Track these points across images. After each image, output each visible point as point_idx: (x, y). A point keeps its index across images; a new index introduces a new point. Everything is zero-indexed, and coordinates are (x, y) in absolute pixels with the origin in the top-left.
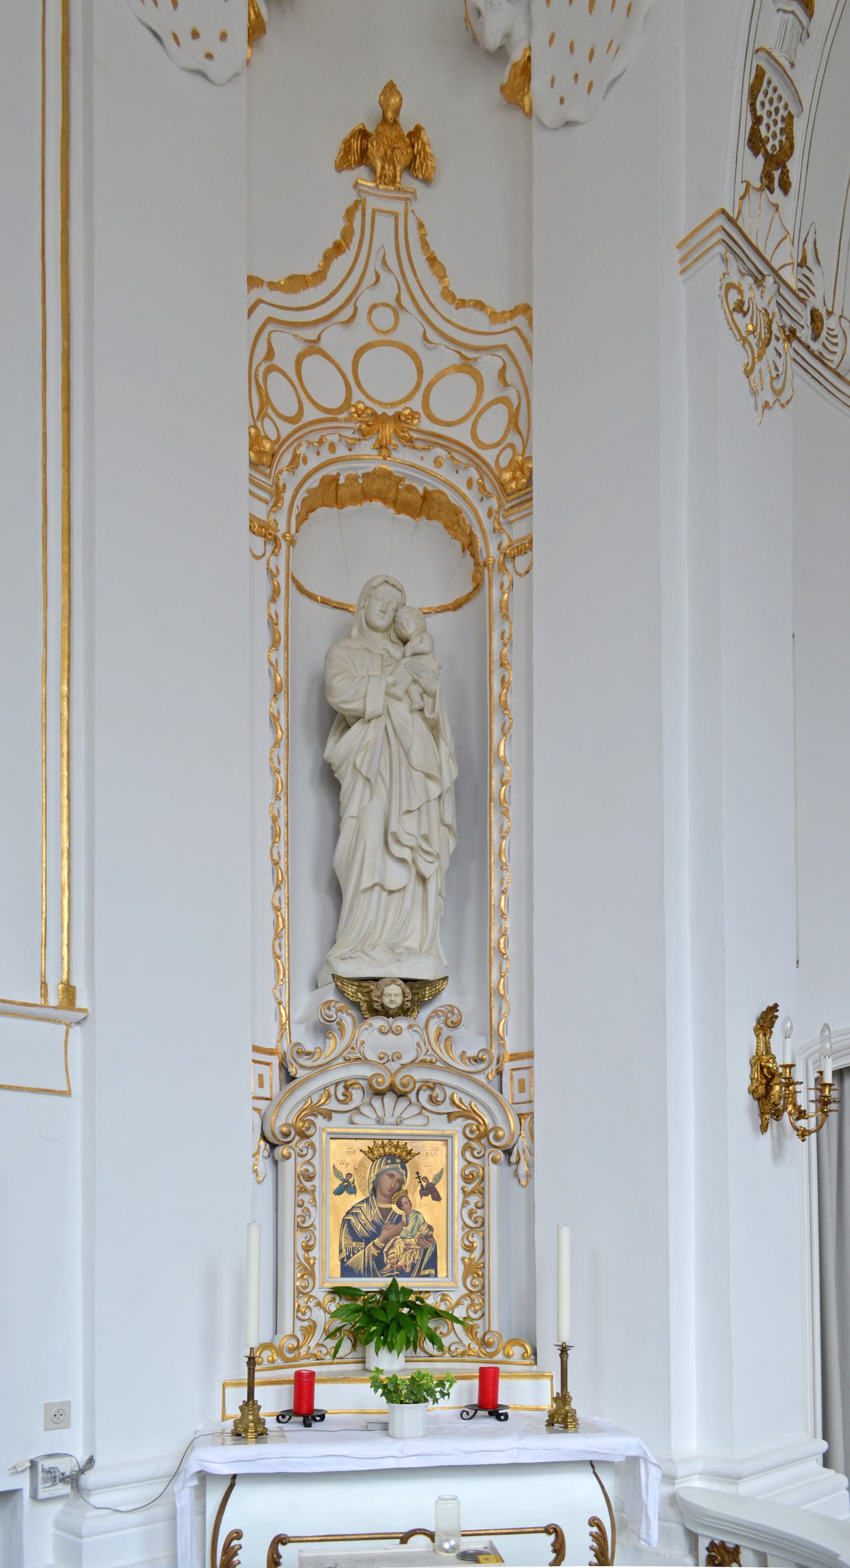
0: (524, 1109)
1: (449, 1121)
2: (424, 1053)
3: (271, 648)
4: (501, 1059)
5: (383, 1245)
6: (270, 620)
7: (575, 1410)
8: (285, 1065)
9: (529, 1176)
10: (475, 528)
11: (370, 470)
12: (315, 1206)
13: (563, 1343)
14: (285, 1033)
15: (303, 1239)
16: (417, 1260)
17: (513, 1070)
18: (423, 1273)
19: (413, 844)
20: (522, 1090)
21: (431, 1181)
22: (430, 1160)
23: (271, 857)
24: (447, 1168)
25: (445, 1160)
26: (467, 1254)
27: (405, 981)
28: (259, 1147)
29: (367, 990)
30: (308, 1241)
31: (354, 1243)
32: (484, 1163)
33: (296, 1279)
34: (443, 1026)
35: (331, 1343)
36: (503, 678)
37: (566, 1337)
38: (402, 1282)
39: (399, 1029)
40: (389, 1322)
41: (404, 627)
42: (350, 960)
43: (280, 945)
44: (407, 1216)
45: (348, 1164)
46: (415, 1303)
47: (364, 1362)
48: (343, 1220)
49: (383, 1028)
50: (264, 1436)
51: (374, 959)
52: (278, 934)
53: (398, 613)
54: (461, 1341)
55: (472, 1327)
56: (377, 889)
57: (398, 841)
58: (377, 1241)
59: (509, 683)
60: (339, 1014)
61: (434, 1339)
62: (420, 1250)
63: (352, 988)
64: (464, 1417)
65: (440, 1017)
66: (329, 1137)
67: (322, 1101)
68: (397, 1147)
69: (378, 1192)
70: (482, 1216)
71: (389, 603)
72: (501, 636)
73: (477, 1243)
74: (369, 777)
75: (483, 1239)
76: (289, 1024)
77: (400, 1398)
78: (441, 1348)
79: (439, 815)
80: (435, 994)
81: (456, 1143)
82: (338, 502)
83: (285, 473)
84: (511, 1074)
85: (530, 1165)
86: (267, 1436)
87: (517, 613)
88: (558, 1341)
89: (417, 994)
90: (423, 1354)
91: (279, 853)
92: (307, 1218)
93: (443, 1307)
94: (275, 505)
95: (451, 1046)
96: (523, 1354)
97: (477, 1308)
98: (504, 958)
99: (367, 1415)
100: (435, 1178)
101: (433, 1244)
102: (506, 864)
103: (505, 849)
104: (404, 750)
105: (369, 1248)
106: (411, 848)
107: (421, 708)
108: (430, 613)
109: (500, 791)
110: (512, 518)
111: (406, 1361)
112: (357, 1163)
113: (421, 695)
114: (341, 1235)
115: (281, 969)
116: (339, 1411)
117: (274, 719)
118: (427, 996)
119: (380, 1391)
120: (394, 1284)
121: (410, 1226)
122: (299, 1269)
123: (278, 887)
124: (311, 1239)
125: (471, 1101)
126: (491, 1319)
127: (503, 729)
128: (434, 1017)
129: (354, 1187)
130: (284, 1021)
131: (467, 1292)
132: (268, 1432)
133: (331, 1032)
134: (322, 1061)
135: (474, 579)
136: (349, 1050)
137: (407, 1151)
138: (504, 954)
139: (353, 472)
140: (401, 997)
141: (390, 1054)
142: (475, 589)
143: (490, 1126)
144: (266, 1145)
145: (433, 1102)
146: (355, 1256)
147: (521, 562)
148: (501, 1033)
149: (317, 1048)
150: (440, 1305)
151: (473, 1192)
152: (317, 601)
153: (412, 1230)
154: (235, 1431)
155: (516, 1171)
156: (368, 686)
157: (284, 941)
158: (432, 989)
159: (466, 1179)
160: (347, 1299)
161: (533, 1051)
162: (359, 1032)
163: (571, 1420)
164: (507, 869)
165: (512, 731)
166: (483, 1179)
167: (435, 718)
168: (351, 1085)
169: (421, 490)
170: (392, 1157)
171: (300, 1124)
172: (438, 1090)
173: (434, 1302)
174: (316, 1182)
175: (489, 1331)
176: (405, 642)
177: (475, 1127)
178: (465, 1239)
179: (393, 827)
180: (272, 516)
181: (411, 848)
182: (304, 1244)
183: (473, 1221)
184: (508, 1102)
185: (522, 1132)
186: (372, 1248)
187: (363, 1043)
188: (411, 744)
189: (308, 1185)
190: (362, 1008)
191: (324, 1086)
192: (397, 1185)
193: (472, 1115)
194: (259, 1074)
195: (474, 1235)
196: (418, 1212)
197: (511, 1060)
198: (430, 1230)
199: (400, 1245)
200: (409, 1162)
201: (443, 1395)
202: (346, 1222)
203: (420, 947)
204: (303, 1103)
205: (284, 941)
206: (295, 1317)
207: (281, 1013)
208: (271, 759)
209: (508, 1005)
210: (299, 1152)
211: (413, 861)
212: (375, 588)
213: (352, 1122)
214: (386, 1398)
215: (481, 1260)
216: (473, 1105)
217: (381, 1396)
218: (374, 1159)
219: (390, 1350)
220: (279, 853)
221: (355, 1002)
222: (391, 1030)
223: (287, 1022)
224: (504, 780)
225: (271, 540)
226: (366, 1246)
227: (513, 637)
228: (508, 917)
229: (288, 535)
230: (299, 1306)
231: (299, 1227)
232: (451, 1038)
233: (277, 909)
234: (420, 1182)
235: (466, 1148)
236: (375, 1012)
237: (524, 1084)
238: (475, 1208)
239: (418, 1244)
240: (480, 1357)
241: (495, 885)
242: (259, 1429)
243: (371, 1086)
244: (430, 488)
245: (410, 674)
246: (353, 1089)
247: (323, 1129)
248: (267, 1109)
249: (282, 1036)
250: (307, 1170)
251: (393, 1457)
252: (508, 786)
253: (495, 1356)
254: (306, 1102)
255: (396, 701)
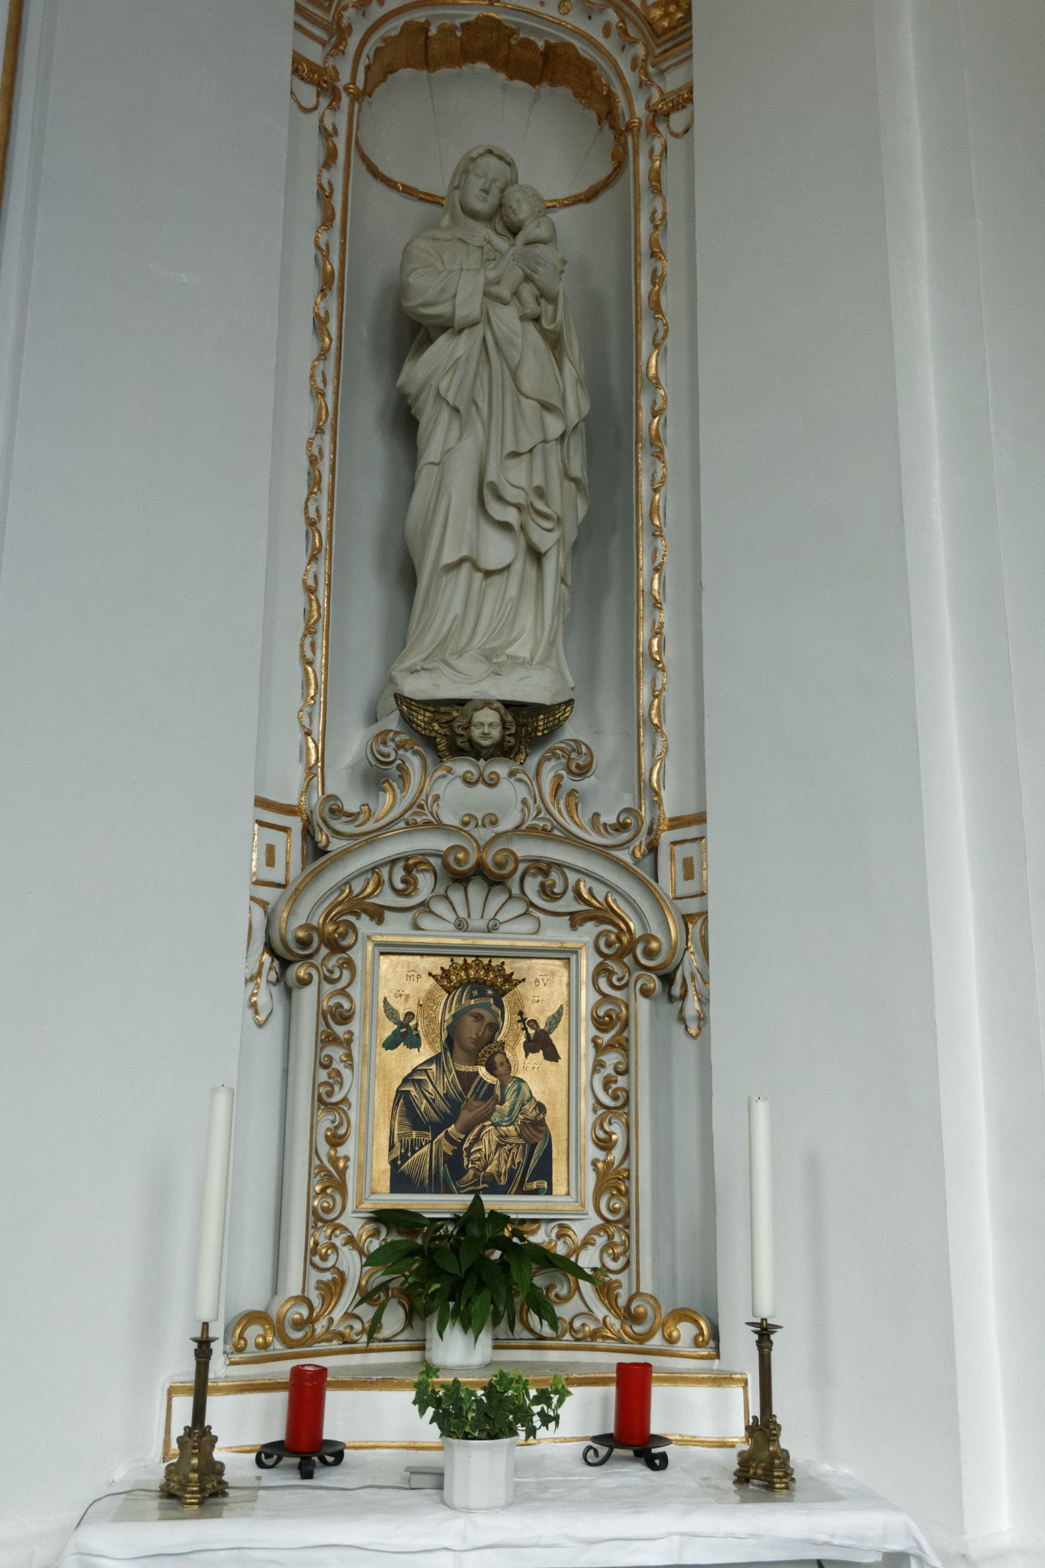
0: (692, 906)
1: (573, 926)
2: (534, 816)
3: (320, 227)
4: (655, 827)
5: (462, 1137)
6: (320, 191)
7: (786, 1452)
8: (311, 832)
9: (702, 1019)
10: (614, 86)
11: (472, 18)
12: (351, 1067)
13: (762, 1320)
14: (315, 778)
15: (328, 1124)
16: (519, 1163)
17: (674, 843)
18: (528, 1186)
19: (521, 500)
20: (689, 875)
21: (542, 1026)
22: (542, 991)
23: (306, 514)
24: (569, 1005)
25: (566, 992)
26: (601, 1155)
27: (508, 705)
28: (261, 965)
29: (448, 718)
30: (337, 1127)
31: (414, 1133)
32: (628, 997)
33: (312, 1194)
34: (563, 773)
35: (367, 1312)
36: (655, 271)
37: (766, 1310)
38: (491, 1202)
39: (494, 776)
40: (462, 1276)
41: (513, 211)
42: (422, 673)
43: (313, 645)
44: (503, 1087)
45: (408, 997)
46: (440, 1241)
47: (423, 1348)
48: (398, 1091)
49: (469, 775)
50: (220, 1500)
51: (457, 671)
52: (310, 627)
53: (506, 193)
54: (591, 1311)
55: (609, 1284)
56: (466, 568)
57: (500, 498)
58: (452, 1129)
59: (663, 278)
60: (401, 752)
61: (545, 1311)
62: (524, 1145)
63: (424, 716)
64: (590, 1460)
65: (559, 758)
66: (377, 950)
67: (369, 890)
68: (488, 968)
69: (456, 1044)
70: (626, 1086)
71: (494, 181)
72: (651, 218)
73: (618, 1133)
74: (457, 405)
75: (628, 1126)
76: (323, 767)
77: (463, 1427)
78: (554, 1322)
79: (561, 464)
80: (554, 726)
81: (584, 963)
82: (427, 62)
83: (351, 11)
84: (671, 849)
85: (703, 1000)
86: (225, 1500)
87: (672, 181)
88: (754, 1315)
89: (525, 725)
90: (526, 1335)
91: (317, 510)
92: (337, 1088)
93: (561, 1249)
94: (336, 47)
95: (576, 805)
96: (696, 1338)
97: (618, 1250)
98: (659, 669)
99: (420, 1452)
100: (550, 1022)
101: (546, 1136)
102: (660, 528)
103: (658, 506)
104: (508, 366)
105: (439, 1142)
106: (518, 507)
107: (536, 317)
108: (554, 207)
109: (650, 424)
110: (664, 66)
111: (495, 1347)
112: (422, 994)
113: (537, 299)
114: (393, 1118)
115: (312, 681)
116: (372, 1444)
117: (320, 324)
118: (541, 728)
119: (430, 1411)
120: (477, 1203)
121: (507, 1104)
122: (318, 1178)
123: (313, 558)
124: (341, 1124)
125: (608, 893)
126: (641, 1271)
127: (654, 341)
128: (549, 759)
129: (418, 1035)
130: (313, 762)
131: (600, 1222)
132: (227, 1491)
133: (387, 781)
134: (370, 826)
135: (613, 156)
136: (415, 809)
137: (504, 976)
138: (659, 662)
139: (448, 21)
140: (499, 728)
141: (480, 817)
142: (615, 169)
143: (638, 932)
144: (273, 961)
145: (548, 896)
146: (415, 1155)
147: (677, 120)
148: (655, 785)
149: (364, 805)
150: (556, 1244)
151: (611, 1046)
152: (397, 189)
153: (512, 1110)
154: (166, 1489)
155: (681, 1010)
156: (458, 283)
157: (320, 640)
158: (549, 718)
159: (600, 1023)
160: (400, 1233)
161: (705, 813)
162: (430, 780)
163: (780, 1474)
164: (662, 536)
165: (666, 342)
166: (626, 1025)
167: (558, 330)
168: (416, 865)
169: (541, 44)
170: (478, 986)
171: (330, 928)
172: (554, 875)
173: (547, 1239)
174: (355, 1026)
175: (638, 1293)
176: (514, 231)
177: (613, 937)
178: (598, 1128)
179: (491, 476)
180: (331, 62)
181: (518, 507)
182: (329, 1133)
183: (611, 1097)
184: (668, 897)
185: (689, 944)
186: (444, 1142)
187: (437, 798)
188: (519, 361)
189: (340, 1030)
190: (439, 747)
191: (373, 866)
192: (488, 1033)
193: (608, 916)
194: (267, 845)
195: (613, 1121)
196: (521, 1080)
197: (671, 828)
198: (540, 1113)
199: (490, 1137)
200: (508, 995)
201: (546, 1420)
202: (402, 1095)
203: (531, 656)
204: (337, 893)
205: (320, 640)
206: (309, 1263)
207: (308, 749)
208: (312, 376)
209: (666, 740)
210: (327, 973)
211: (522, 528)
212: (473, 160)
213: (416, 927)
214: (440, 1428)
215: (625, 1166)
216: (610, 900)
217: (431, 1423)
218: (451, 989)
219: (465, 1329)
220: (317, 510)
221: (428, 737)
222: (481, 779)
223: (320, 764)
224: (656, 409)
225: (326, 90)
226: (434, 1137)
227: (668, 217)
228: (664, 606)
229: (351, 86)
230: (316, 1244)
231: (322, 1102)
232: (577, 792)
233: (311, 591)
234: (525, 1029)
235: (601, 970)
236: (457, 751)
237: (692, 866)
238: (614, 1074)
239: (520, 1136)
240: (621, 1340)
241: (645, 561)
242: (209, 1486)
243: (446, 865)
244: (553, 41)
245: (520, 268)
246: (418, 871)
247: (369, 938)
248: (278, 902)
249: (308, 785)
250: (340, 1006)
251: (447, 1549)
252: (663, 417)
253: (648, 1339)
254: (343, 892)
255: (501, 305)
